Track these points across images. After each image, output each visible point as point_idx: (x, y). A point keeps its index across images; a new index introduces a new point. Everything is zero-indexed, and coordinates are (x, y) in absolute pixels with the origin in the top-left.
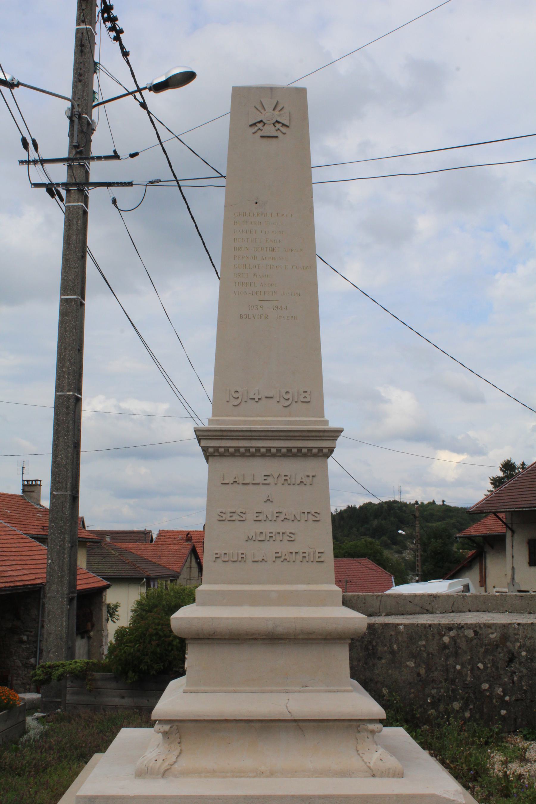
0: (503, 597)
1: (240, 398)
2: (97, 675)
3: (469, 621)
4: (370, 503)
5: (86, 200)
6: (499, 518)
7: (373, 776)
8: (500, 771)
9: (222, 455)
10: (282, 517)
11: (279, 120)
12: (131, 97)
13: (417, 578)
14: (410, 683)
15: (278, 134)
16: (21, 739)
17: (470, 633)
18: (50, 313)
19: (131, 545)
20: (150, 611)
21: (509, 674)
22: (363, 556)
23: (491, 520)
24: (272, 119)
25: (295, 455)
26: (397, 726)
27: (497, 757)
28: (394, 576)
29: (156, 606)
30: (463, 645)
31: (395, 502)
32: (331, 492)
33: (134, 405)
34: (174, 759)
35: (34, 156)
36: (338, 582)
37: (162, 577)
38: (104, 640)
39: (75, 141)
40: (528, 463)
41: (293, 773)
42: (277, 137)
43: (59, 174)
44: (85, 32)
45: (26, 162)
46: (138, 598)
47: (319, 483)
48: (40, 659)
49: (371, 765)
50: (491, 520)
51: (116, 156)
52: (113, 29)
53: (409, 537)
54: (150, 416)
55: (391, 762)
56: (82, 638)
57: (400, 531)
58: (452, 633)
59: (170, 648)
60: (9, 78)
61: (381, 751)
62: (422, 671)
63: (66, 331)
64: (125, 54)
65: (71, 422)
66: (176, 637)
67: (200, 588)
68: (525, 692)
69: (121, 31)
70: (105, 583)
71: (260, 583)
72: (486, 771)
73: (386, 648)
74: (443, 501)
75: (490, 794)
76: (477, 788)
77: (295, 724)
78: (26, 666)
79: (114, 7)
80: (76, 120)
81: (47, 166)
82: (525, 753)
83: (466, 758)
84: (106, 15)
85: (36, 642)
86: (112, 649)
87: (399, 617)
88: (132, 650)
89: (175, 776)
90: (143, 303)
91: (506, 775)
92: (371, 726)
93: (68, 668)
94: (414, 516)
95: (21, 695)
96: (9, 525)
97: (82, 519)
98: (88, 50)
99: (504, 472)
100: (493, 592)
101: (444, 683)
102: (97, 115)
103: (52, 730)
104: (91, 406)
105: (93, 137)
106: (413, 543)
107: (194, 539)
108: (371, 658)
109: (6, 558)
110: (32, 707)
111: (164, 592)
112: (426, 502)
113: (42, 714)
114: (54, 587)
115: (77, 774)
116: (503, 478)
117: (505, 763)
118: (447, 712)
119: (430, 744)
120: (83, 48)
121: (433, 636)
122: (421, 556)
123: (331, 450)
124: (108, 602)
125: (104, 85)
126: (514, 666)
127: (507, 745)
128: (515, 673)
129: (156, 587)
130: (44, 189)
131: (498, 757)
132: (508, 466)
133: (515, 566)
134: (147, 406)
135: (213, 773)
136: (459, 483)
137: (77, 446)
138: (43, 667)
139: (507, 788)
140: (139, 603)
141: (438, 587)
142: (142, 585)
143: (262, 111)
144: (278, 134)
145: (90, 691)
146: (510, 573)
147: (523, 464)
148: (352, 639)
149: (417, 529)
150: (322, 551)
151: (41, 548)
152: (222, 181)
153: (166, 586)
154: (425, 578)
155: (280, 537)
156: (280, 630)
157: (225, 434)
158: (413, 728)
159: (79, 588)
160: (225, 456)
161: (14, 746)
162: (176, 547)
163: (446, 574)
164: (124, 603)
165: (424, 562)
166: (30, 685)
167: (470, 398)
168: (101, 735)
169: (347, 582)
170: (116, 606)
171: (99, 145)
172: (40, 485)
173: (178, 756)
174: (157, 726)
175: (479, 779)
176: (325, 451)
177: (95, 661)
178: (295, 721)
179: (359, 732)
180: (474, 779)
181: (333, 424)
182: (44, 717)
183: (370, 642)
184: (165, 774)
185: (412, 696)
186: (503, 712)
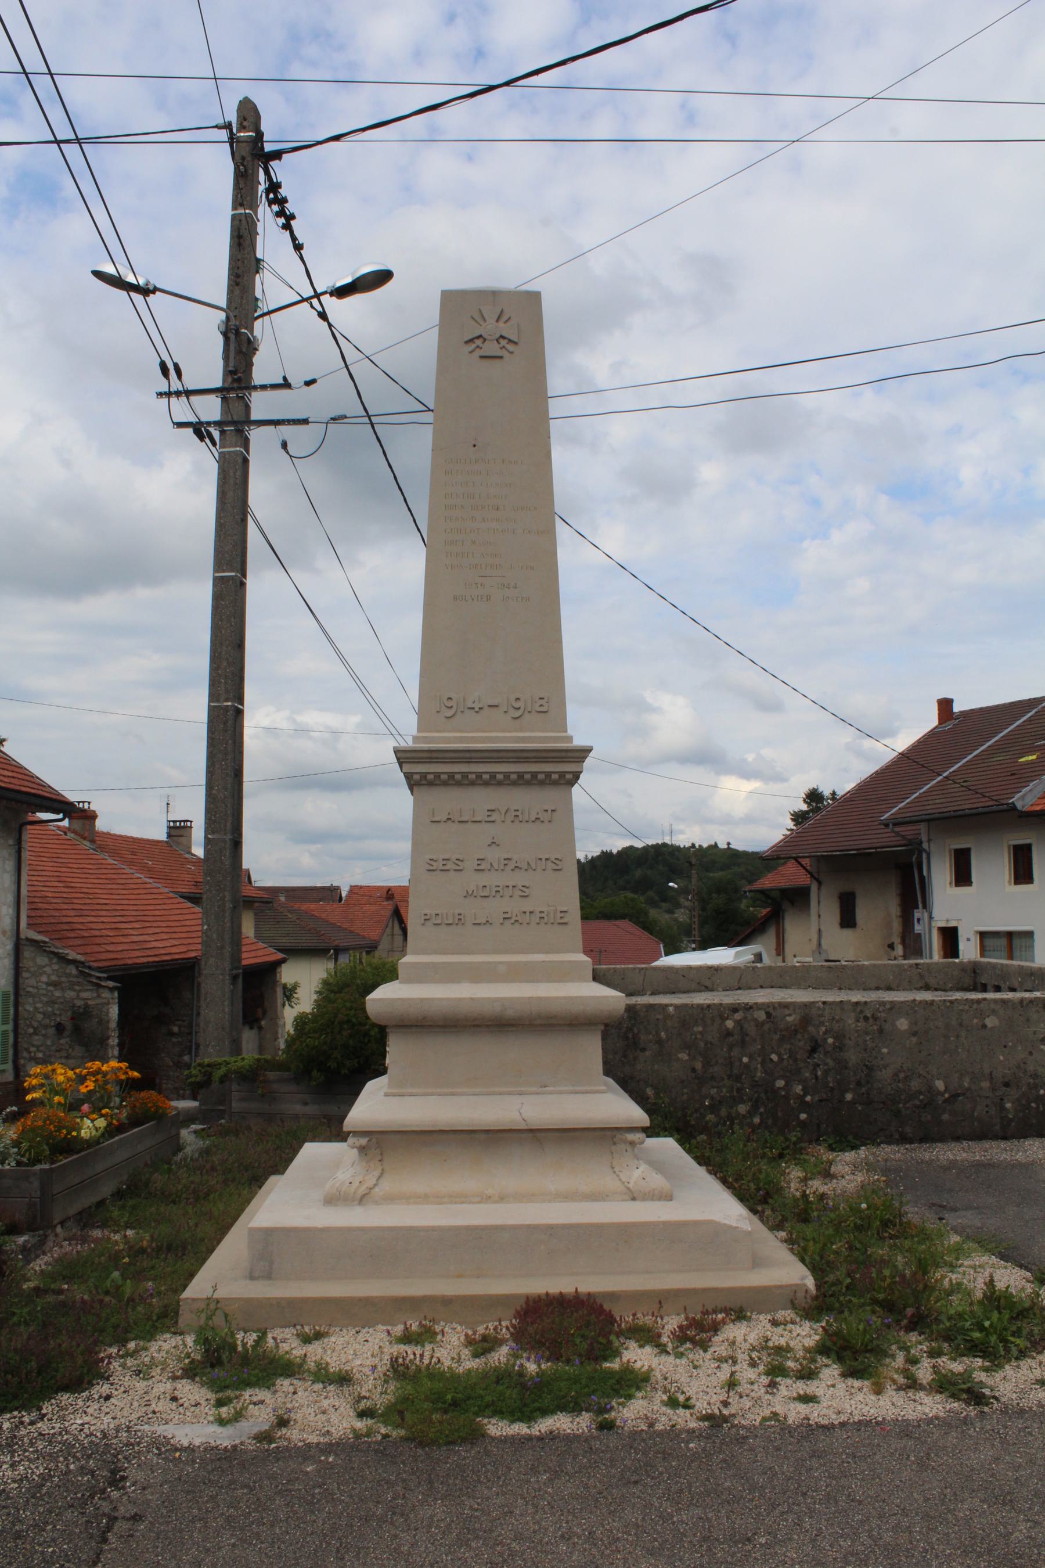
0: (806, 968)
1: (455, 707)
2: (271, 1075)
3: (760, 1000)
4: (631, 847)
5: (246, 443)
6: (802, 865)
7: (634, 1199)
8: (797, 1190)
9: (431, 784)
10: (512, 865)
11: (504, 334)
12: (306, 304)
13: (693, 946)
14: (682, 1082)
15: (503, 353)
16: (175, 1158)
17: (761, 1016)
18: (199, 596)
19: (313, 906)
20: (340, 992)
21: (811, 1068)
22: (623, 917)
23: (791, 868)
24: (495, 337)
25: (528, 783)
26: (666, 1136)
27: (793, 1173)
28: (664, 943)
29: (348, 986)
30: (751, 1030)
31: (664, 845)
32: (578, 834)
33: (312, 718)
34: (374, 1181)
35: (176, 385)
36: (587, 951)
37: (354, 948)
38: (280, 1031)
39: (231, 364)
40: (840, 793)
41: (528, 1197)
42: (501, 357)
43: (211, 409)
44: (243, 218)
45: (165, 393)
46: (324, 975)
47: (561, 818)
48: (196, 1056)
49: (630, 1186)
50: (791, 868)
51: (286, 385)
52: (281, 214)
53: (683, 891)
54: (335, 732)
55: (657, 1181)
56: (251, 1028)
57: (671, 884)
58: (738, 1016)
59: (366, 1040)
60: (142, 282)
61: (643, 1167)
62: (698, 1066)
63: (221, 620)
64: (298, 247)
65: (230, 742)
66: (374, 1025)
67: (403, 960)
68: (832, 1089)
69: (292, 217)
70: (280, 956)
71: (485, 952)
72: (779, 1190)
73: (651, 1037)
74: (729, 844)
75: (784, 1219)
76: (768, 1212)
77: (530, 1135)
78: (179, 1065)
79: (283, 185)
80: (232, 337)
81: (193, 399)
82: (830, 1167)
83: (754, 1174)
84: (271, 196)
85: (190, 1033)
86: (291, 1042)
87: (669, 996)
88: (317, 1043)
89: (376, 1203)
90: (326, 581)
91: (804, 1195)
92: (630, 1137)
93: (233, 1067)
94: (690, 863)
95: (174, 1103)
96: (151, 881)
97: (248, 871)
98: (248, 242)
99: (809, 804)
100: (795, 962)
101: (726, 1081)
102: (260, 328)
103: (215, 1146)
104: (257, 720)
105: (256, 359)
106: (688, 899)
107: (397, 897)
108: (628, 1049)
109: (148, 924)
110: (188, 1119)
111: (358, 967)
112: (705, 845)
113: (202, 1127)
114: (212, 961)
115: (248, 1202)
116: (807, 812)
117: (805, 1180)
118: (731, 1118)
119: (708, 1158)
120: (242, 241)
121: (713, 1020)
122: (699, 916)
123: (576, 776)
124: (284, 981)
125: (270, 289)
126: (818, 1057)
127: (807, 1157)
128: (818, 1065)
129: (344, 960)
130: (191, 430)
131: (796, 1173)
132: (814, 797)
133: (822, 929)
134: (331, 720)
135: (424, 1199)
136: (749, 820)
137: (238, 773)
138: (199, 1065)
139: (805, 1211)
140: (325, 983)
141: (721, 956)
142: (330, 958)
143: (481, 322)
144: (503, 353)
145: (263, 1096)
146: (815, 937)
147: (834, 793)
148: (606, 1025)
149: (694, 881)
150: (565, 909)
151: (193, 910)
152: (429, 417)
153: (360, 959)
154: (704, 945)
155: (510, 891)
156: (510, 1013)
157: (435, 755)
158: (686, 1140)
159: (244, 963)
160: (436, 785)
161: (166, 1167)
162: (373, 908)
163: (732, 940)
164: (305, 982)
165: (702, 925)
166: (184, 1090)
167: (769, 706)
168: (278, 1152)
169: (601, 952)
170: (295, 986)
171: (263, 370)
172: (191, 827)
173: (379, 1177)
174: (351, 1140)
175: (770, 1201)
176: (569, 776)
177: (268, 1057)
178: (531, 1131)
179: (615, 1144)
180: (764, 1201)
181: (579, 741)
182: (203, 1130)
183: (631, 1029)
184: (362, 1200)
185: (685, 1097)
186: (803, 1116)
